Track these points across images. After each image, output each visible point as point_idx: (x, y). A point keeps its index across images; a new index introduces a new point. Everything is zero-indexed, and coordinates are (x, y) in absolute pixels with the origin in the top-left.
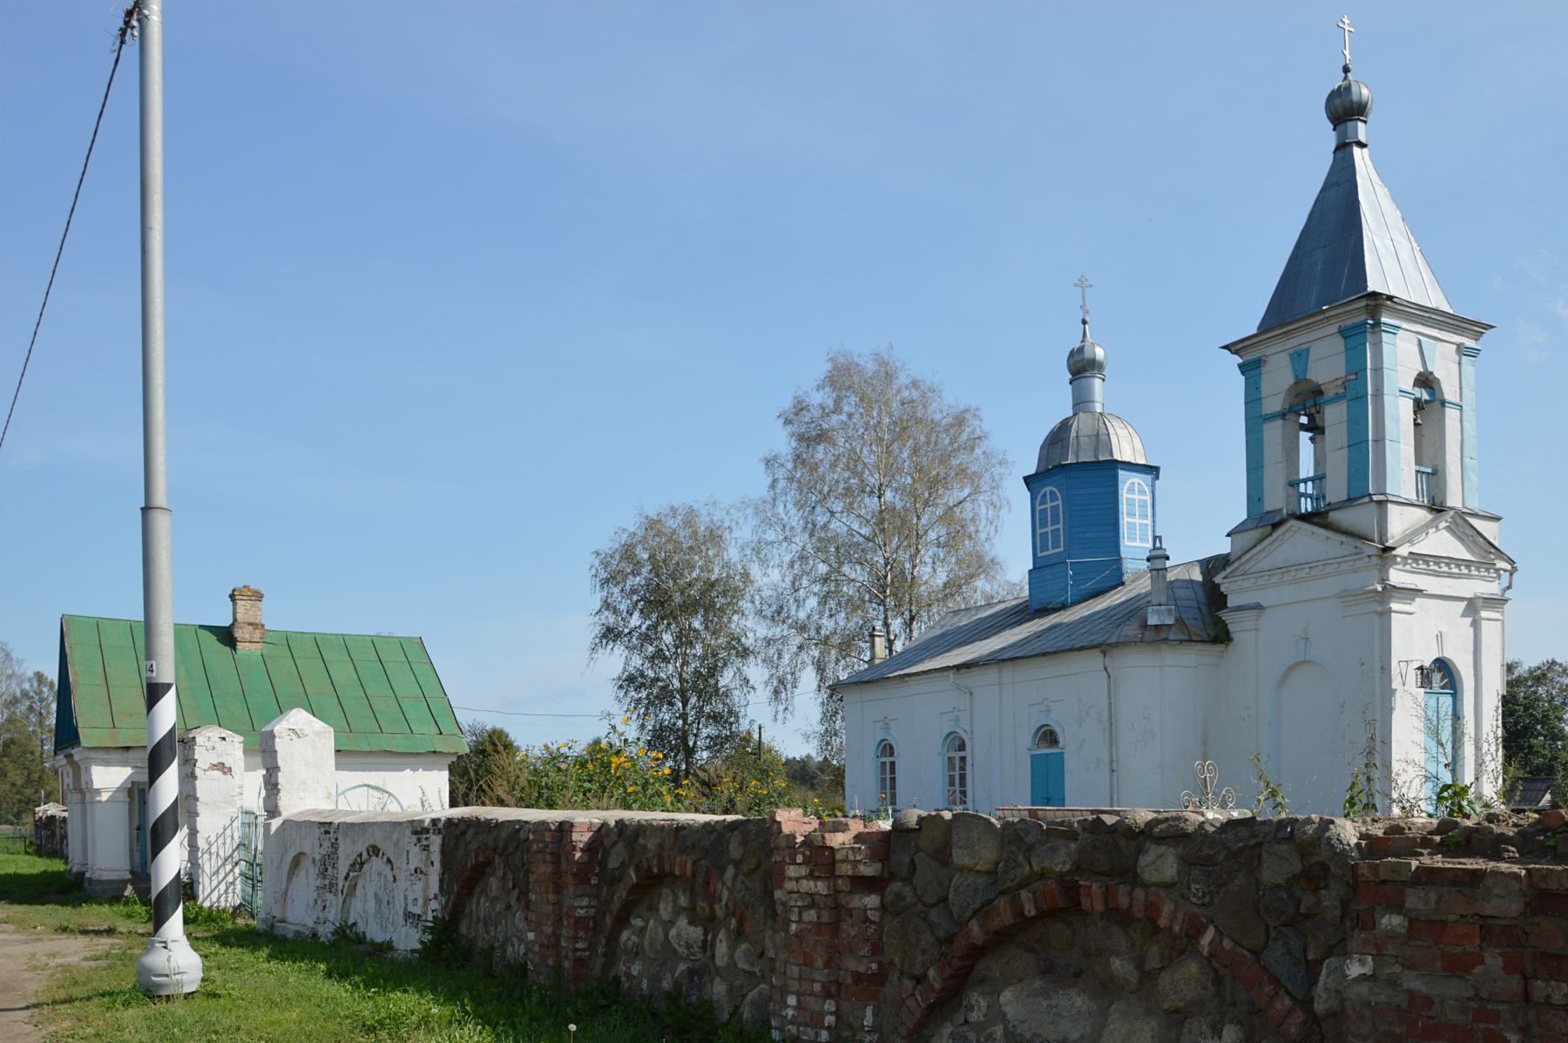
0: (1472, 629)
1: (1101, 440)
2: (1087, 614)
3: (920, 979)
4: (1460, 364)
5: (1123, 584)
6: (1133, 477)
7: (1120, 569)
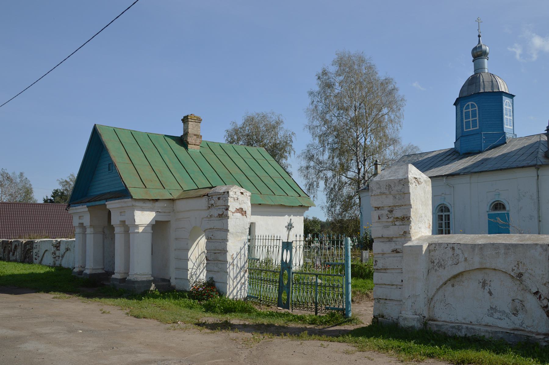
1: (493, 83)
2: (500, 154)
3: (533, 321)
5: (506, 143)
6: (507, 99)
7: (505, 136)
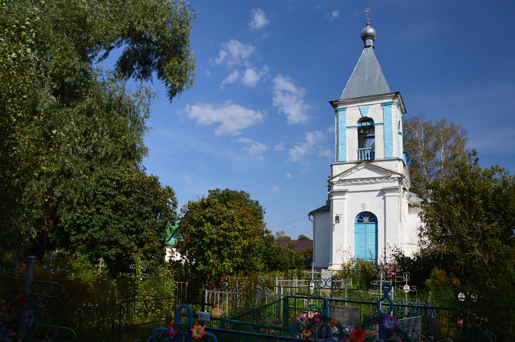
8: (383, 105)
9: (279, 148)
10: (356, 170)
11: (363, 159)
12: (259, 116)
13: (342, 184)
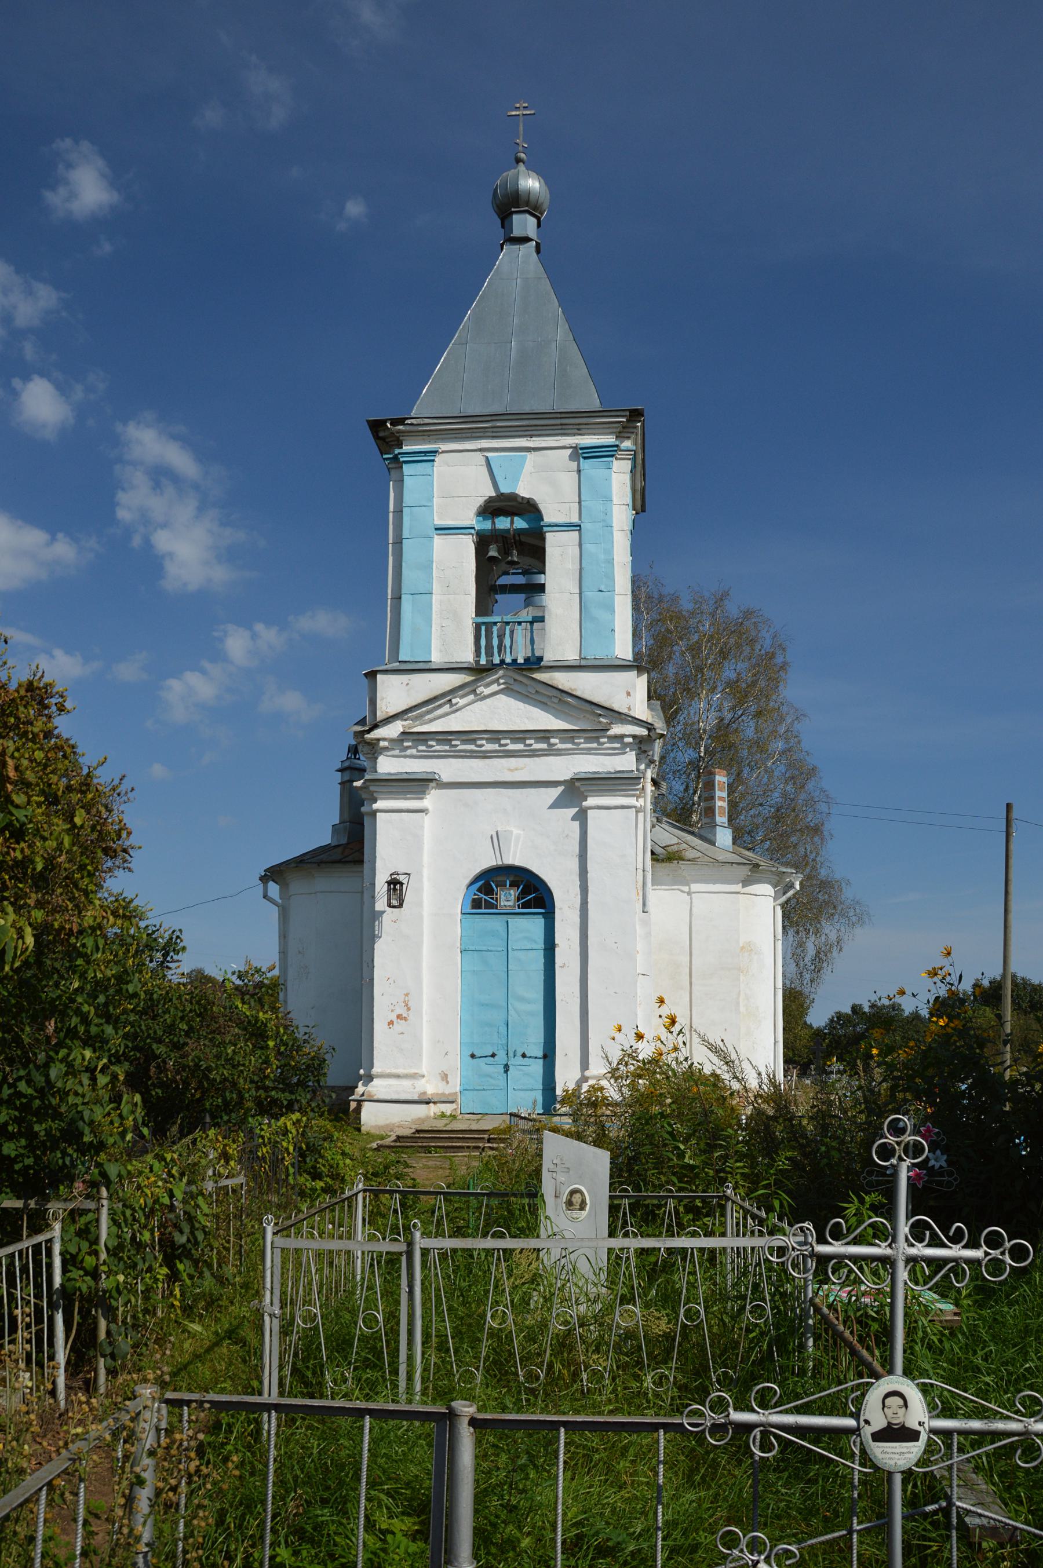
0: (576, 824)
4: (579, 471)
8: (581, 454)
9: (128, 671)
10: (472, 697)
11: (497, 660)
12: (64, 550)
13: (414, 751)
